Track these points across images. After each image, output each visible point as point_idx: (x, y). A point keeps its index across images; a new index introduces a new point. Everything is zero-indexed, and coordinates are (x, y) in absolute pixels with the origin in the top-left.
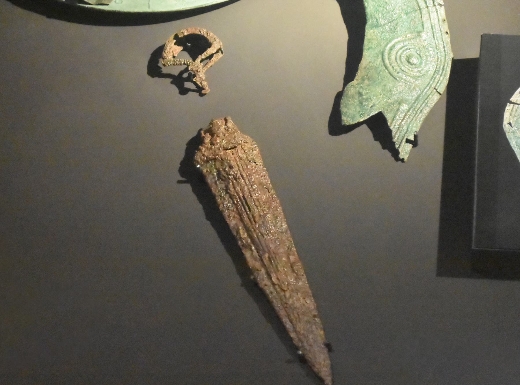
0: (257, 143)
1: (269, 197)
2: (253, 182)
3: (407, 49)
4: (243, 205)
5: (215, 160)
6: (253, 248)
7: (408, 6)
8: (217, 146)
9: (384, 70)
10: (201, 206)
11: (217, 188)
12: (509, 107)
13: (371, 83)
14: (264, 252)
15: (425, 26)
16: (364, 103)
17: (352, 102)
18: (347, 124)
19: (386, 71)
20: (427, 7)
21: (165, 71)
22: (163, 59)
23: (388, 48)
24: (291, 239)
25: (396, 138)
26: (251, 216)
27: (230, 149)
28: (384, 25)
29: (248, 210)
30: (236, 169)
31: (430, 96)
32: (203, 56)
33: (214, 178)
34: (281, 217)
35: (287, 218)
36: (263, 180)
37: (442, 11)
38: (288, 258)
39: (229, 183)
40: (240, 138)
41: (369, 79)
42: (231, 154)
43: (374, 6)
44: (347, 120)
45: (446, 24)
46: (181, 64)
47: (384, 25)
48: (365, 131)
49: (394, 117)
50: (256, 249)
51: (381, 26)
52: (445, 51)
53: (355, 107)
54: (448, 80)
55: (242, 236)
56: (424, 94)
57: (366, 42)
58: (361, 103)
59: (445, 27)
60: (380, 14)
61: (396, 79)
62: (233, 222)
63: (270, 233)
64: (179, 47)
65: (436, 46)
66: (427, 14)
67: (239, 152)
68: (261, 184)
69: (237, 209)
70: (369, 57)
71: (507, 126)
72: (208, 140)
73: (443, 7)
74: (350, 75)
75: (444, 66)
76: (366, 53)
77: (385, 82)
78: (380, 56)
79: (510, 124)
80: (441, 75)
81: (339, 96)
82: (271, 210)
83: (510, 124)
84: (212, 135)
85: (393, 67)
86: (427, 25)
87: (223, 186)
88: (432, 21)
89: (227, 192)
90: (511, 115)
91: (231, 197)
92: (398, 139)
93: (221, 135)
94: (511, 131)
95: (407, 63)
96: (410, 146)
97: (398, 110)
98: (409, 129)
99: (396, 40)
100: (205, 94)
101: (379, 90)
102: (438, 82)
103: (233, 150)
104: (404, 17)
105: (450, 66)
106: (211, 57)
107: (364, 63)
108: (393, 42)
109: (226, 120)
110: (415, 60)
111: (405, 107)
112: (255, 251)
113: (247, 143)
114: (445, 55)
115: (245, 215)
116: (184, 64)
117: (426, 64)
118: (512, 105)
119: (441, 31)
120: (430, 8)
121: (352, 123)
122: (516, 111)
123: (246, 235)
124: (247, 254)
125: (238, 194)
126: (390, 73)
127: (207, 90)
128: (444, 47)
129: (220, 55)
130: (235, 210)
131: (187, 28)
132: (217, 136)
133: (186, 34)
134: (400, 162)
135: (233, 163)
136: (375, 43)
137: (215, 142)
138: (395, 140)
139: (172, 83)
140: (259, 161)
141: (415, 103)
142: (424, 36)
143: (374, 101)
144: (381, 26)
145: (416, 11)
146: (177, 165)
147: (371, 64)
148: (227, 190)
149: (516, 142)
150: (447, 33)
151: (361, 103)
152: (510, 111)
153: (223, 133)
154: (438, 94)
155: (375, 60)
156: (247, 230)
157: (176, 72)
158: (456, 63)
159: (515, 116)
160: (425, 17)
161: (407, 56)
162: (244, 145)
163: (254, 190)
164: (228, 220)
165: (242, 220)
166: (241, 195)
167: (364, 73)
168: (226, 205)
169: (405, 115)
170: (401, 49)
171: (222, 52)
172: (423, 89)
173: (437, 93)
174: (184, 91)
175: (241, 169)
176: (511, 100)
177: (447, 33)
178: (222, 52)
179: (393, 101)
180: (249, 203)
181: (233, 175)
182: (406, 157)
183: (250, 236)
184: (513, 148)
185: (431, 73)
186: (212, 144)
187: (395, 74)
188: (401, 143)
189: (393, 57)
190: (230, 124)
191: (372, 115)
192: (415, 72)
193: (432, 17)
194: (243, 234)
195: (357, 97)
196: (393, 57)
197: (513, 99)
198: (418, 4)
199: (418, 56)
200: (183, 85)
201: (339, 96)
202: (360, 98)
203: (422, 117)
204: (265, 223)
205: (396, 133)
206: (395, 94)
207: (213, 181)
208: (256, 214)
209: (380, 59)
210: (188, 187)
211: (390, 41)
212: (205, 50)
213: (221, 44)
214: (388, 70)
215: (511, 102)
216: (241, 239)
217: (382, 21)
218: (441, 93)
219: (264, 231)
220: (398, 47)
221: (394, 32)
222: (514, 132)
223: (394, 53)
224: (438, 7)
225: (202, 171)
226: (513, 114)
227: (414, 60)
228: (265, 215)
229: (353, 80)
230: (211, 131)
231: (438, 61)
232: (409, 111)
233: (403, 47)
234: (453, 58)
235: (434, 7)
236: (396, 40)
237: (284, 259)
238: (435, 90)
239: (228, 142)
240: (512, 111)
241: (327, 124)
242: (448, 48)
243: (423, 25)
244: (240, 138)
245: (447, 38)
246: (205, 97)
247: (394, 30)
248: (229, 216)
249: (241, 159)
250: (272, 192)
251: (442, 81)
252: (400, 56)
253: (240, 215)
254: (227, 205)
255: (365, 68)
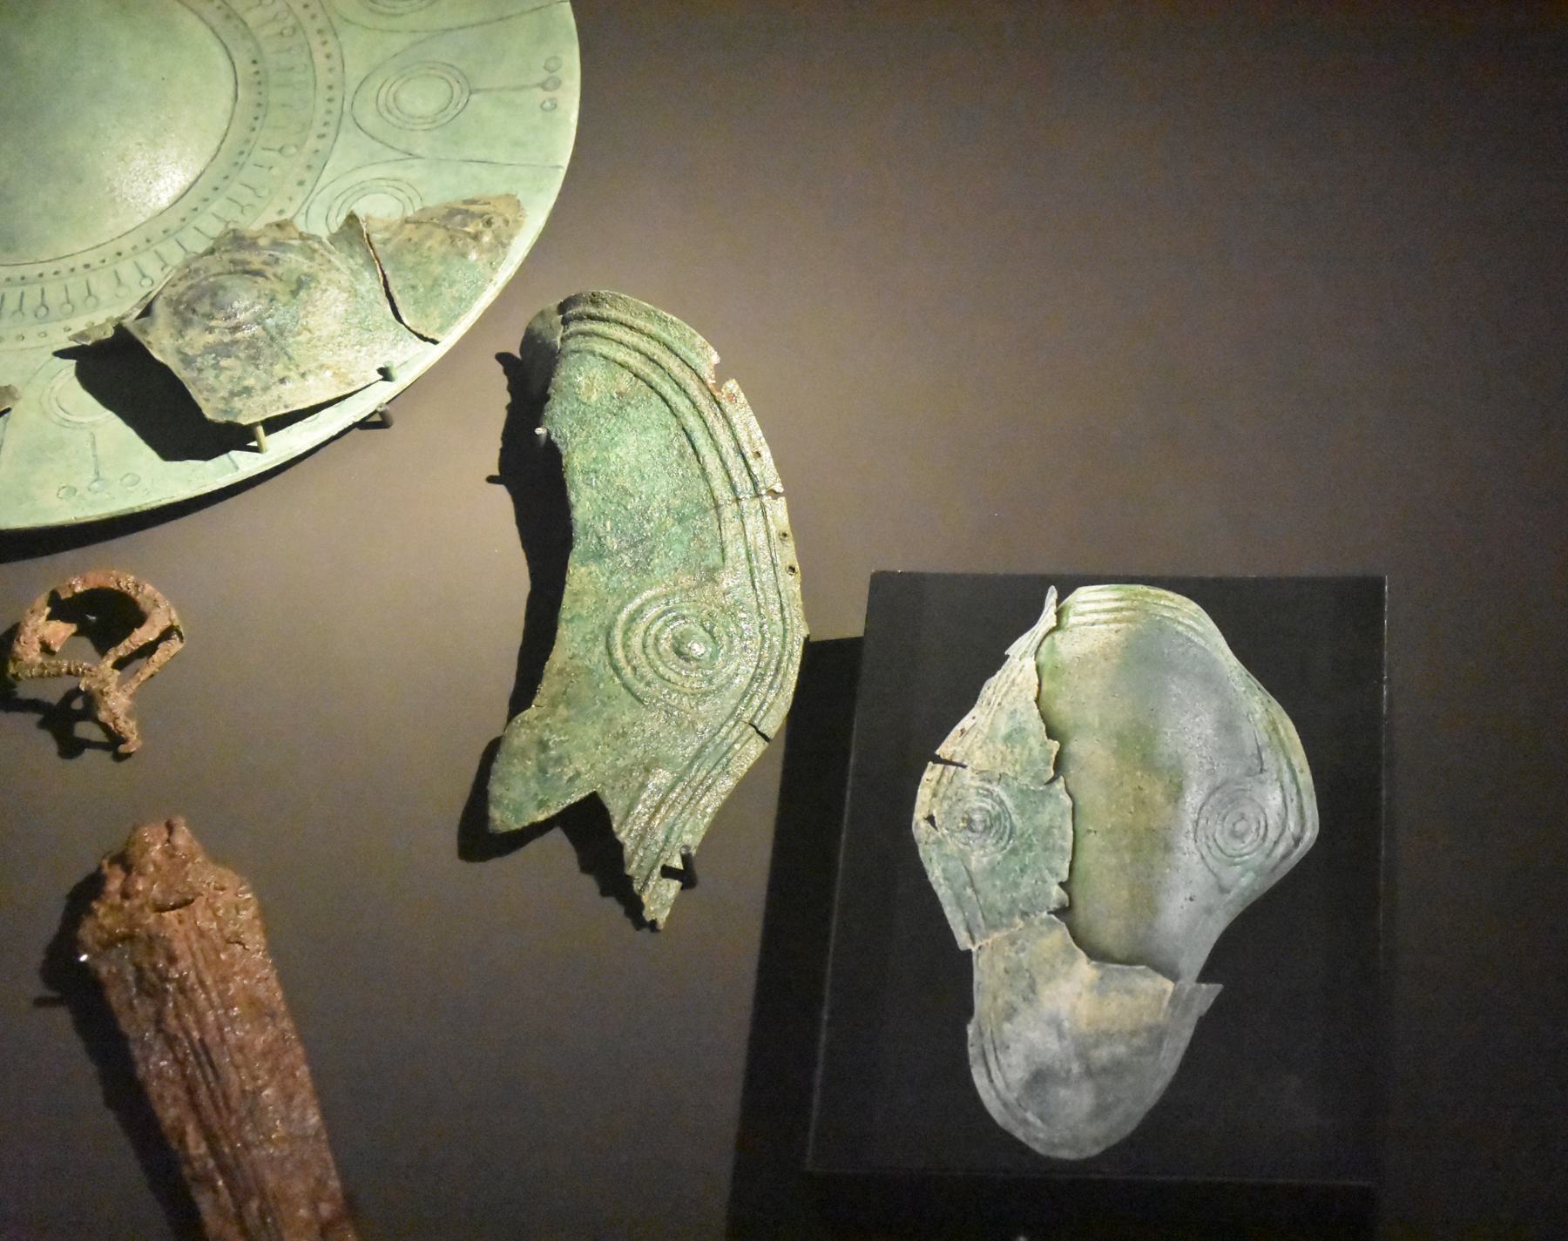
0: (255, 889)
1: (276, 1040)
2: (232, 998)
3: (676, 618)
4: (200, 1064)
5: (129, 938)
6: (220, 1183)
7: (684, 499)
8: (137, 902)
9: (611, 678)
10: (91, 1069)
11: (135, 1020)
12: (931, 773)
13: (573, 712)
14: (249, 1195)
15: (730, 551)
16: (551, 771)
17: (520, 768)
18: (503, 829)
19: (617, 680)
20: (738, 500)
21: (25, 691)
22: (15, 660)
23: (623, 616)
24: (328, 1156)
25: (634, 866)
26: (218, 1094)
27: (173, 908)
28: (618, 552)
29: (211, 1077)
30: (182, 965)
31: (737, 746)
32: (123, 649)
33: (127, 989)
34: (304, 1094)
35: (321, 1093)
36: (261, 992)
37: (779, 512)
38: (315, 1209)
39: (165, 1003)
40: (205, 876)
41: (568, 704)
42: (175, 922)
43: (593, 501)
44: (503, 819)
45: (791, 544)
46: (59, 675)
47: (618, 552)
48: (559, 847)
49: (631, 807)
50: (228, 1185)
51: (611, 554)
52: (783, 619)
53: (526, 782)
54: (791, 698)
55: (193, 1152)
56: (718, 740)
57: (567, 600)
58: (543, 770)
59: (788, 554)
60: (608, 524)
61: (641, 702)
62: (170, 1113)
63: (270, 1140)
64: (68, 625)
65: (759, 606)
66: (737, 521)
67: (199, 914)
68: (253, 1002)
69: (184, 1076)
70: (572, 640)
71: (924, 825)
72: (114, 885)
73: (782, 501)
74: (522, 696)
75: (779, 662)
76: (564, 632)
77: (611, 710)
78: (602, 638)
79: (931, 819)
80: (771, 687)
81: (492, 750)
82: (278, 1076)
83: (931, 819)
84: (128, 869)
85: (634, 669)
86: (735, 550)
87: (151, 1010)
88: (750, 538)
89: (159, 1031)
90: (934, 795)
91: (171, 1041)
92: (639, 867)
93: (151, 869)
94: (932, 838)
95: (673, 656)
96: (675, 885)
97: (643, 786)
98: (673, 839)
99: (648, 594)
100: (129, 755)
101: (594, 732)
102: (760, 707)
103: (181, 911)
104: (676, 529)
105: (797, 659)
106: (148, 649)
107: (558, 657)
108: (638, 601)
109: (170, 828)
110: (696, 646)
111: (662, 777)
112: (225, 1194)
113: (223, 889)
114: (785, 630)
115: (203, 1092)
116: (69, 673)
117: (729, 659)
118: (939, 767)
119: (774, 566)
120: (744, 503)
121: (516, 826)
122: (951, 782)
123: (203, 1149)
124: (204, 1202)
125: (187, 1033)
126: (626, 686)
127: (134, 743)
128: (782, 609)
129: (175, 646)
130: (179, 1078)
131: (80, 574)
132: (141, 874)
133: (79, 589)
134: (646, 931)
135: (179, 947)
136: (589, 600)
137: (131, 890)
138: (631, 870)
139: (42, 725)
140: (255, 941)
141: (690, 766)
142: (727, 581)
143: (580, 764)
144: (611, 554)
145: (706, 511)
146: (37, 958)
147: (577, 662)
148: (159, 1020)
149: (944, 870)
150: (792, 569)
151: (543, 770)
152: (933, 783)
153: (155, 865)
154: (761, 740)
155: (588, 650)
156: (210, 1137)
157: (53, 694)
158: (813, 650)
159: (945, 797)
160: (730, 531)
161: (674, 637)
162: (216, 896)
163: (232, 1021)
164: (158, 1108)
165: (195, 1107)
166: (196, 1035)
167: (556, 688)
168: (156, 1064)
169: (662, 801)
170: (659, 617)
171: (180, 635)
172: (717, 725)
173: (757, 736)
174: (71, 748)
175: (201, 964)
176: (938, 752)
177: (792, 569)
178: (180, 635)
179: (628, 761)
180: (214, 1058)
181: (177, 980)
182: (662, 918)
183: (214, 1151)
184: (935, 887)
185: (741, 682)
186: (125, 895)
187: (640, 687)
188: (648, 878)
189: (636, 642)
190: (182, 838)
191: (570, 801)
192: (695, 681)
193: (749, 528)
194: (196, 1146)
195: (533, 755)
196: (636, 642)
197: (944, 750)
198: (711, 491)
199: (707, 636)
200: (70, 730)
201: (492, 750)
202: (542, 756)
203: (711, 803)
204: (257, 1114)
205: (635, 852)
206: (636, 744)
207: (124, 997)
208: (234, 1091)
209: (602, 648)
210: (62, 1018)
211: (631, 598)
212: (127, 633)
213: (174, 615)
214: (619, 676)
215: (938, 760)
216: (189, 1160)
217: (612, 543)
218: (771, 735)
219: (250, 1137)
220: (651, 613)
221: (645, 571)
222: (939, 843)
223: (640, 628)
224: (767, 499)
225: (97, 972)
226: (942, 790)
227: (698, 649)
228: (257, 1092)
229: (529, 706)
230: (125, 861)
231: (762, 648)
232: (672, 788)
233: (664, 613)
234: (807, 640)
235: (757, 501)
236: (648, 594)
237: (303, 1212)
238: (751, 730)
239: (169, 889)
240: (938, 782)
241: (455, 829)
242: (796, 612)
243: (723, 550)
244: (205, 876)
245: (792, 586)
246: (125, 764)
247: (642, 568)
248: (161, 1097)
249: (202, 934)
250: (286, 1024)
251: (772, 704)
252: (657, 639)
253: (191, 1091)
254: (156, 1064)
255: (560, 672)
